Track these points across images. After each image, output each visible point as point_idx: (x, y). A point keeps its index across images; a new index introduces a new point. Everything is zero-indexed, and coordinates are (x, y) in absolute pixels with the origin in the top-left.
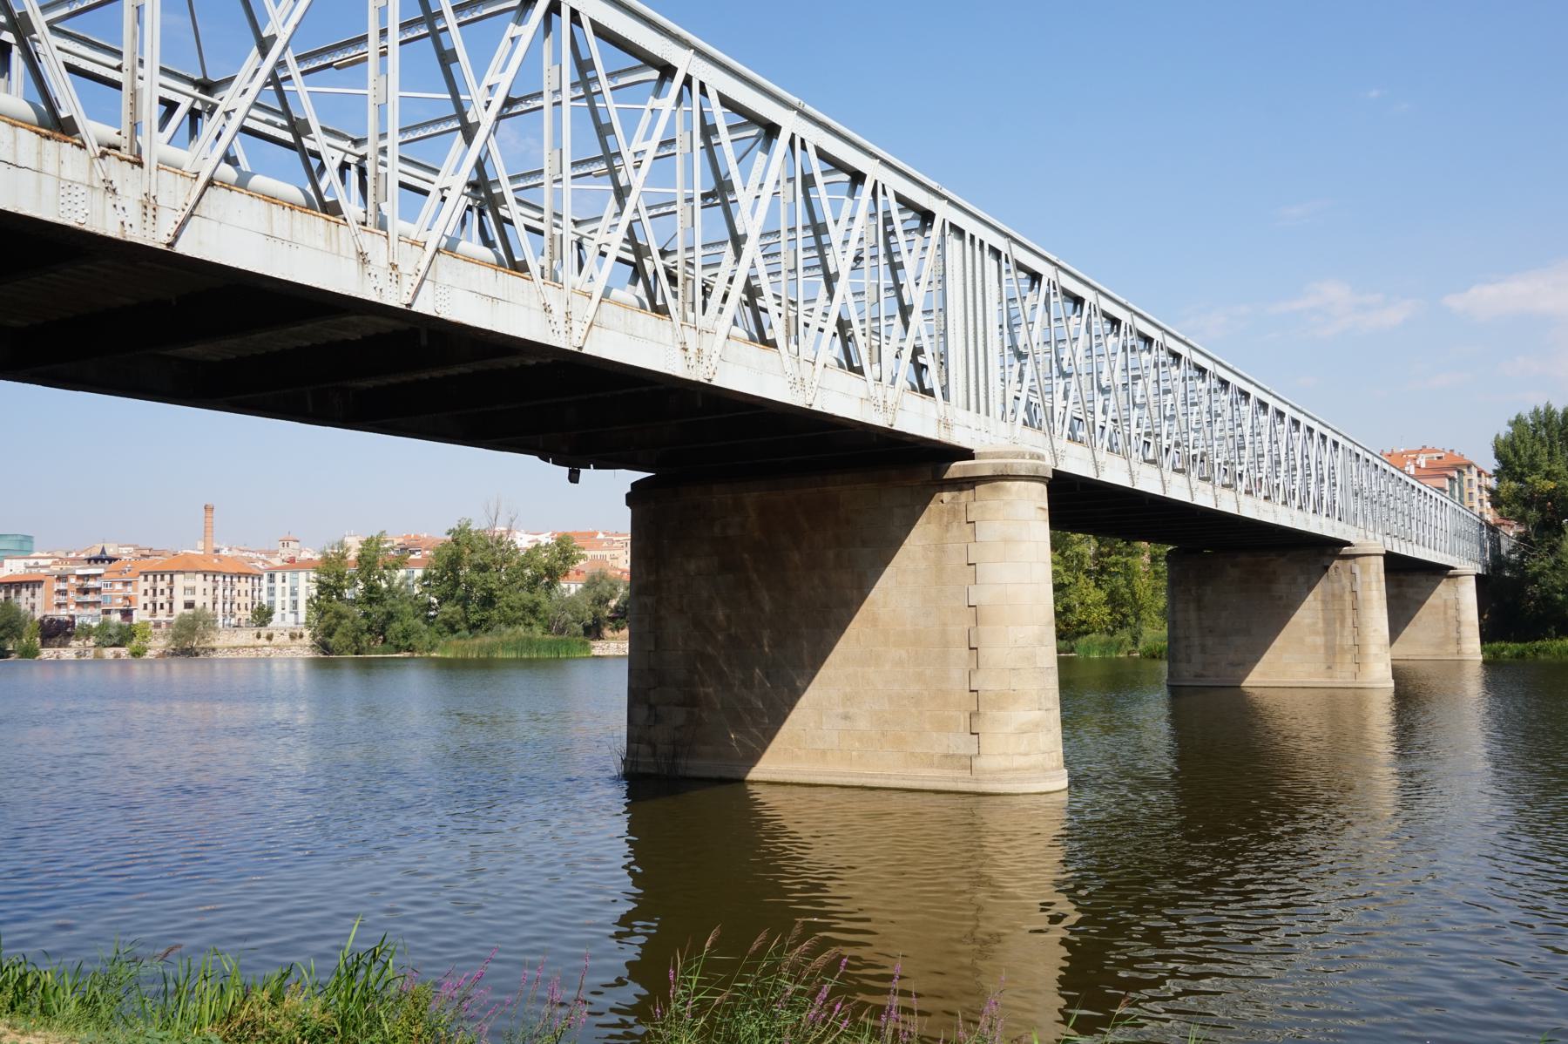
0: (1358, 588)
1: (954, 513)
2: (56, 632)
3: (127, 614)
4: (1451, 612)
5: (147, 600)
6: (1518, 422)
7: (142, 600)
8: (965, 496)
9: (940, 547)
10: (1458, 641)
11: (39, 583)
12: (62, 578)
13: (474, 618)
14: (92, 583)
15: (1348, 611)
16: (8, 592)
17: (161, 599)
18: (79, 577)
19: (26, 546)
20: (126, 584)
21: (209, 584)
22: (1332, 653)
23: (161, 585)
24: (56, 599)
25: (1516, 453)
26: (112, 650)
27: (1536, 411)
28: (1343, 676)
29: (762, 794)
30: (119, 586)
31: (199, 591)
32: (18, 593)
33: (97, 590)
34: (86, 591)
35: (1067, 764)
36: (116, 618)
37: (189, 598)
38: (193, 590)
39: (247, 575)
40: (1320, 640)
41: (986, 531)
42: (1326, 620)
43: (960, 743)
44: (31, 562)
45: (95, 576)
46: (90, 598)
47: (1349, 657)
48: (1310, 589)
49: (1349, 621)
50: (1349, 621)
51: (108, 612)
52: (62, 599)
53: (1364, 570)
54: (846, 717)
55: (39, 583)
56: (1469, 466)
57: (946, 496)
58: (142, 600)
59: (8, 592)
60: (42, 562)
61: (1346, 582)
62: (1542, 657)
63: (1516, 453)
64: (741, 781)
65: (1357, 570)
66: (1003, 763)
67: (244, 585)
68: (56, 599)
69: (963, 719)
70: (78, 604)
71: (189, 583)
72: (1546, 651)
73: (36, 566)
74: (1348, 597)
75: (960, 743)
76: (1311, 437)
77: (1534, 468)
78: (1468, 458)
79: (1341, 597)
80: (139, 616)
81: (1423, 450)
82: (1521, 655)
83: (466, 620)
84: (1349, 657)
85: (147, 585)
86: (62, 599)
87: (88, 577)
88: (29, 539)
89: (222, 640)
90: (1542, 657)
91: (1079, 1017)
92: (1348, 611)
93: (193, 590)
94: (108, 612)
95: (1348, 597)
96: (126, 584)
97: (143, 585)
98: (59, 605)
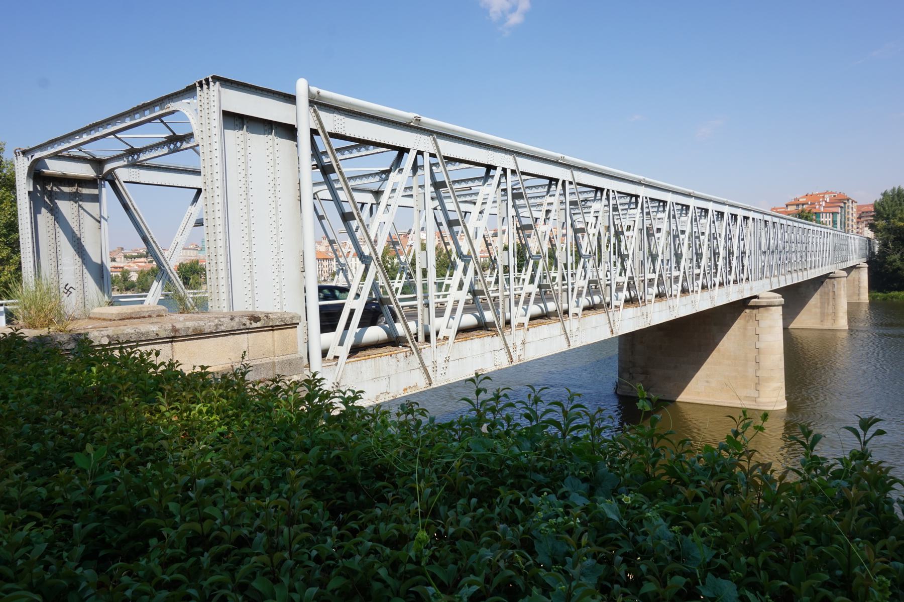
0: (835, 290)
1: (751, 317)
4: (856, 283)
6: (885, 194)
8: (755, 311)
9: (745, 328)
10: (859, 295)
15: (831, 299)
22: (823, 316)
25: (884, 209)
27: (894, 189)
28: (827, 325)
29: (680, 405)
35: (787, 398)
40: (818, 310)
41: (763, 324)
42: (821, 303)
43: (753, 393)
47: (830, 317)
48: (816, 290)
49: (831, 303)
50: (831, 303)
53: (839, 283)
54: (707, 382)
56: (848, 200)
57: (748, 311)
61: (830, 288)
62: (894, 300)
63: (884, 209)
64: (673, 402)
65: (835, 283)
66: (768, 400)
69: (753, 386)
72: (897, 298)
74: (831, 294)
75: (753, 393)
77: (894, 215)
78: (849, 196)
79: (828, 294)
81: (827, 192)
82: (885, 299)
84: (830, 317)
90: (894, 300)
92: (831, 299)
95: (831, 294)
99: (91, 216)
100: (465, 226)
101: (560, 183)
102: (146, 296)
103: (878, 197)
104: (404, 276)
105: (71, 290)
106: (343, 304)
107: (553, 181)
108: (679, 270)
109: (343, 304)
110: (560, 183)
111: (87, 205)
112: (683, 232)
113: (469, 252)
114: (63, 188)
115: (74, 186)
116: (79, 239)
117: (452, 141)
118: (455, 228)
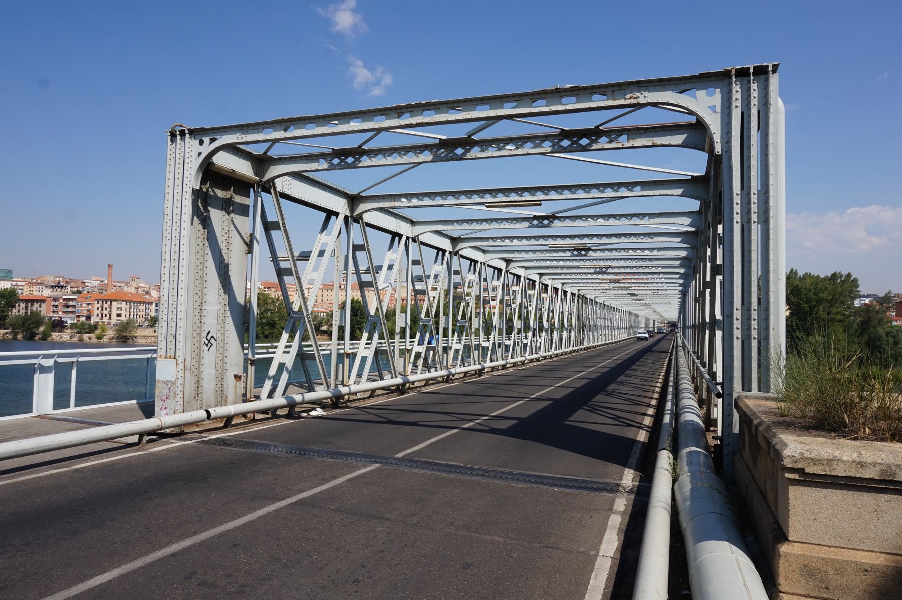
2: (59, 325)
3: (88, 318)
5: (98, 312)
7: (96, 312)
11: (44, 301)
12: (55, 299)
13: (266, 332)
14: (71, 303)
16: (27, 304)
17: (105, 312)
18: (64, 300)
19: (9, 275)
20: (88, 304)
21: (128, 306)
23: (105, 306)
24: (52, 309)
26: (87, 335)
30: (85, 305)
31: (124, 309)
32: (32, 305)
33: (74, 306)
34: (68, 306)
36: (83, 319)
37: (119, 312)
38: (121, 308)
39: (143, 302)
44: (14, 283)
45: (72, 300)
46: (70, 309)
51: (78, 316)
52: (55, 309)
55: (44, 301)
58: (96, 312)
59: (27, 304)
60: (19, 284)
67: (142, 307)
68: (52, 309)
70: (63, 312)
71: (119, 305)
73: (16, 285)
76: (557, 294)
80: (94, 319)
83: (263, 333)
85: (99, 305)
86: (55, 309)
87: (69, 300)
88: (10, 272)
89: (140, 332)
91: (69, 407)
93: (121, 308)
94: (78, 316)
96: (88, 304)
97: (96, 305)
98: (53, 312)
99: (240, 235)
100: (298, 278)
101: (404, 238)
102: (274, 353)
103: (824, 272)
104: (376, 336)
105: (212, 340)
106: (272, 358)
107: (396, 235)
108: (488, 341)
109: (272, 358)
110: (404, 238)
111: (238, 219)
112: (494, 299)
113: (300, 307)
114: (217, 191)
115: (227, 189)
116: (227, 266)
117: (330, 192)
118: (286, 279)
